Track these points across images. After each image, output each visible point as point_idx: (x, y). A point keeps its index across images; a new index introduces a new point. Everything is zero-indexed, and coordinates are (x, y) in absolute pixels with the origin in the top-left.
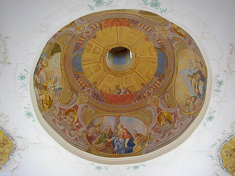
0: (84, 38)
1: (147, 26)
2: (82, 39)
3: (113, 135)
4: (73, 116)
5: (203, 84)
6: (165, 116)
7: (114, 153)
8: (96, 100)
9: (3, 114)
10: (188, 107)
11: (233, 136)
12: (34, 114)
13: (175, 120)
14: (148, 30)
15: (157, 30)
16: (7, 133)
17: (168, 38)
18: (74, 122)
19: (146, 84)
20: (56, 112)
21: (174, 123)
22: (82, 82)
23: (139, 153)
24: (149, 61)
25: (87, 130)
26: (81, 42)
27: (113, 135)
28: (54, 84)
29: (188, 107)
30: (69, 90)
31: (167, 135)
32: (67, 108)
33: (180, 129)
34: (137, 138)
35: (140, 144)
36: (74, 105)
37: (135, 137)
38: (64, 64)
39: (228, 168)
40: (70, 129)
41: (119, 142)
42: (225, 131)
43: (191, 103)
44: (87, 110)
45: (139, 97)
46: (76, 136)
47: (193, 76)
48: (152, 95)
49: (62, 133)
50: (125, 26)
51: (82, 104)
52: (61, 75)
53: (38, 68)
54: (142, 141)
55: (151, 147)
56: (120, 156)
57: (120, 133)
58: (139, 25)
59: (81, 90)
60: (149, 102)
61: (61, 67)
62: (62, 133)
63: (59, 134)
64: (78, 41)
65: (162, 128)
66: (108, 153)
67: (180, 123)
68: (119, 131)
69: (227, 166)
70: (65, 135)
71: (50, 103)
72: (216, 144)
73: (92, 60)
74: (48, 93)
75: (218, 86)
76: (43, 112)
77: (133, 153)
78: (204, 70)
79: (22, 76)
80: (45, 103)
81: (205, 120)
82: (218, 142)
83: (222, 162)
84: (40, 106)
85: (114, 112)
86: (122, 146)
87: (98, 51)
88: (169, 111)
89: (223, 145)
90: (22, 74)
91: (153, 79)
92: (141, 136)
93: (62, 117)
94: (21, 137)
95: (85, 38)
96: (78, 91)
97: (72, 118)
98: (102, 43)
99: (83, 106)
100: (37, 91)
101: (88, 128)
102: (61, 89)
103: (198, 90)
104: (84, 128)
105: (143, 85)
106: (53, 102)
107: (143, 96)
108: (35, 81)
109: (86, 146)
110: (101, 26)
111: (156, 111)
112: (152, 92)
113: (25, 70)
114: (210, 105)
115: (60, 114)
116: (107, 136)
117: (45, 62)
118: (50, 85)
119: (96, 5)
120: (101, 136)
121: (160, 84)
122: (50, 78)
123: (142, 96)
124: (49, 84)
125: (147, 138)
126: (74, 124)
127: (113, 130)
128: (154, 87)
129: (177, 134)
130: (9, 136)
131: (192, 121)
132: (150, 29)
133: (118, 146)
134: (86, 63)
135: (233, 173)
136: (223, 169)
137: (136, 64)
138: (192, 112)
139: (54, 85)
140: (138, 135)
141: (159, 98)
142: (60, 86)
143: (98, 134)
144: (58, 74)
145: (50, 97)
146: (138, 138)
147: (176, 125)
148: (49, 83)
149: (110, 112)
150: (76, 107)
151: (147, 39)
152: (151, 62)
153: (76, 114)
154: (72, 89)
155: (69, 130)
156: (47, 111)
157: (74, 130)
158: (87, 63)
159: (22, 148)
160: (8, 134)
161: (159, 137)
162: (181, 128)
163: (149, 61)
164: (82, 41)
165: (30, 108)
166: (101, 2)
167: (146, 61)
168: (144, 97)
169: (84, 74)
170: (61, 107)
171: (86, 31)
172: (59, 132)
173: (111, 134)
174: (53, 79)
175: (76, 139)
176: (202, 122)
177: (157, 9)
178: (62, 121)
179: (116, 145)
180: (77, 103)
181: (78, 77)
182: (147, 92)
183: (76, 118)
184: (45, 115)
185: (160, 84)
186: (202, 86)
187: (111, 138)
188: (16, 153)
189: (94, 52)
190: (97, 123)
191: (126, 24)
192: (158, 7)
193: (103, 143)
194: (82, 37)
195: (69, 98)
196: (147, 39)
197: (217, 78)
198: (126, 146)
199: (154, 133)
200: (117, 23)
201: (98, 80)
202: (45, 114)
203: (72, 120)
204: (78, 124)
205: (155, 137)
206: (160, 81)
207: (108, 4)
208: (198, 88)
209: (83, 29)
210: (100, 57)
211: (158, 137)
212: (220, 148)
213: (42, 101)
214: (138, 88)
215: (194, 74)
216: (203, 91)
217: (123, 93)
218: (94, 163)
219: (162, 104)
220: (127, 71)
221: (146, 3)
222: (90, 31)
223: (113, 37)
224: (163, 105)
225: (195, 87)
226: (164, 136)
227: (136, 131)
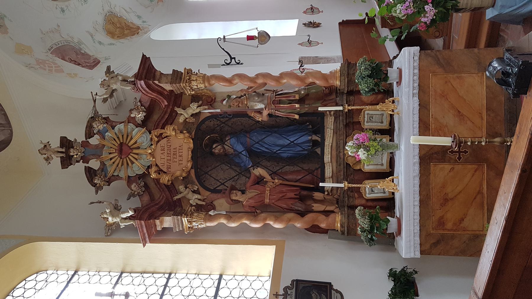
94: (103, 6)
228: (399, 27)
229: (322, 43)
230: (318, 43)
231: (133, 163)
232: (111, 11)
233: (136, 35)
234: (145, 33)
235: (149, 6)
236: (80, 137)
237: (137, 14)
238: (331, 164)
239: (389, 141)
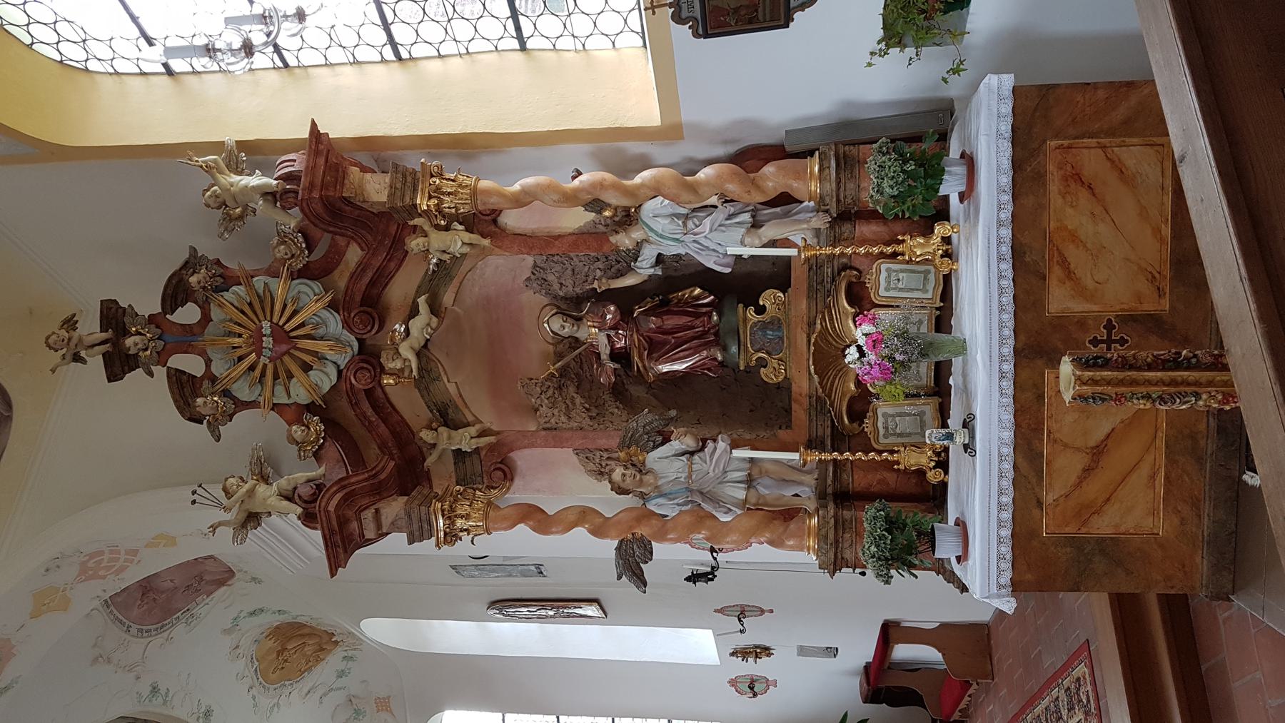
11: (254, 656)
39: (306, 667)
69: (300, 670)
72: (254, 698)
83: (289, 680)
89: (261, 679)
212: (264, 687)
228: (922, 709)
229: (771, 611)
230: (763, 612)
231: (290, 376)
236: (149, 304)
239: (936, 332)
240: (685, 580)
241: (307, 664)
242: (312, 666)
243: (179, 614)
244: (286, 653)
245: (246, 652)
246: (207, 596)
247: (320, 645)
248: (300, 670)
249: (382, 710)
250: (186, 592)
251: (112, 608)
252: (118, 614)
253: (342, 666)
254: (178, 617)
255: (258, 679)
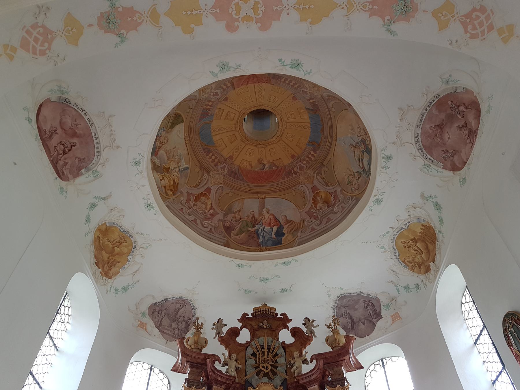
0: (213, 102)
1: (293, 82)
2: (210, 104)
3: (257, 223)
4: (206, 202)
5: (369, 158)
6: (322, 197)
7: (259, 245)
8: (233, 179)
9: (117, 207)
10: (350, 185)
11: (410, 223)
12: (155, 205)
13: (335, 202)
14: (296, 86)
15: (307, 86)
16: (123, 230)
17: (322, 96)
18: (206, 210)
19: (296, 155)
20: (183, 199)
21: (333, 206)
22: (213, 157)
23: (290, 245)
24: (299, 126)
25: (224, 218)
26: (208, 107)
27: (257, 223)
28: (178, 163)
29: (350, 185)
30: (197, 169)
31: (325, 221)
32: (197, 192)
33: (341, 213)
34: (287, 225)
35: (291, 233)
36: (206, 187)
37: (285, 224)
38: (188, 137)
39: (407, 263)
40: (202, 218)
41: (265, 231)
42: (399, 217)
43: (355, 181)
44: (222, 193)
45: (289, 173)
46: (210, 227)
47: (356, 145)
48: (305, 170)
49: (192, 225)
50: (265, 82)
51: (216, 185)
52: (186, 152)
53: (156, 147)
54: (293, 230)
55: (305, 237)
56: (266, 250)
57: (266, 220)
58: (283, 80)
59: (213, 168)
60: (302, 179)
61: (185, 140)
62: (193, 225)
63: (189, 226)
64: (205, 107)
65: (318, 213)
66: (251, 247)
67: (340, 206)
68: (264, 217)
69: (405, 259)
70: (196, 226)
71: (175, 188)
72: (388, 233)
73: (224, 129)
74: (172, 176)
75: (386, 161)
76: (167, 201)
77: (282, 245)
78: (368, 139)
79: (136, 161)
80: (168, 190)
81: (370, 203)
82: (391, 231)
83: (399, 255)
84: (162, 194)
85: (257, 193)
86: (268, 236)
87: (232, 116)
88: (327, 190)
89: (398, 234)
90: (136, 159)
91: (306, 149)
92: (292, 223)
93: (192, 204)
94: (142, 234)
95: (214, 101)
96: (210, 169)
97: (203, 203)
98: (236, 106)
99: (217, 188)
100: (157, 176)
101: (225, 215)
102: (187, 168)
103: (363, 164)
104: (220, 216)
105: (293, 156)
106: (179, 187)
107: (294, 171)
108: (153, 163)
109: (223, 238)
110: (233, 85)
111: (310, 190)
112: (305, 166)
113: (140, 154)
114: (376, 186)
115: (188, 200)
116: (249, 224)
117: (164, 138)
118: (172, 166)
119: (220, 70)
120: (242, 224)
121: (315, 155)
122: (173, 157)
123: (293, 172)
124: (171, 164)
125: (300, 225)
126: (207, 211)
127: (256, 216)
128: (307, 159)
129: (338, 220)
130: (127, 233)
131: (355, 204)
132: (298, 85)
133: (263, 236)
134: (217, 133)
135: (413, 269)
136: (401, 264)
137: (283, 130)
138: (355, 192)
139: (178, 165)
140: (288, 221)
141: (314, 173)
142: (186, 166)
143: (238, 223)
144: (182, 150)
145: (174, 181)
146: (289, 226)
147: (336, 208)
148: (171, 163)
149: (252, 193)
150: (209, 190)
151: (294, 98)
152: (302, 127)
153: (208, 198)
154: (202, 167)
155: (201, 220)
156: (171, 199)
157: (208, 219)
158: (219, 132)
159: (144, 246)
160: (125, 231)
161: (315, 224)
162: (342, 213)
163: (299, 126)
164: (211, 106)
165: (150, 199)
166: (226, 67)
167: (296, 126)
168: (295, 173)
169: (216, 147)
170: (190, 191)
171: (213, 93)
172: (188, 224)
173: (255, 222)
174: (177, 157)
175: (211, 231)
176: (367, 206)
177: (299, 70)
178: (191, 210)
179: (261, 235)
180: (209, 185)
181: (209, 152)
182: (298, 166)
183: (209, 203)
184: (170, 205)
185: (315, 155)
186: (367, 159)
187: (254, 226)
188: (137, 252)
189: (227, 119)
190: (236, 208)
191: (266, 81)
192: (300, 69)
193: (244, 233)
194: (209, 101)
195: (199, 178)
196: (294, 98)
197: (383, 152)
198: (274, 236)
199: (307, 218)
200: (253, 80)
201: (235, 154)
202: (169, 203)
203: (204, 206)
204: (212, 211)
205: (310, 224)
206: (315, 151)
207: (236, 69)
208: (362, 162)
209: (209, 91)
210: (235, 124)
211: (314, 224)
212: (394, 238)
213: (165, 187)
214: (287, 161)
215: (357, 143)
216: (369, 167)
217: (268, 169)
218: (234, 259)
219: (319, 180)
220: (272, 140)
221: (284, 64)
222: (219, 93)
223: (250, 98)
224: (320, 182)
225: (359, 161)
226: (321, 222)
227: (286, 217)
232: (136, 246)
233: (93, 261)
234: (94, 273)
235: (137, 308)
237: (130, 287)
238: (246, 371)
240: (363, 368)
241: (409, 262)
242: (408, 266)
243: (429, 157)
244: (414, 244)
245: (412, 216)
246: (443, 168)
247: (423, 263)
248: (405, 259)
249: (393, 318)
250: (444, 152)
251: (429, 109)
252: (425, 115)
253: (412, 286)
254: (427, 157)
255: (398, 232)
